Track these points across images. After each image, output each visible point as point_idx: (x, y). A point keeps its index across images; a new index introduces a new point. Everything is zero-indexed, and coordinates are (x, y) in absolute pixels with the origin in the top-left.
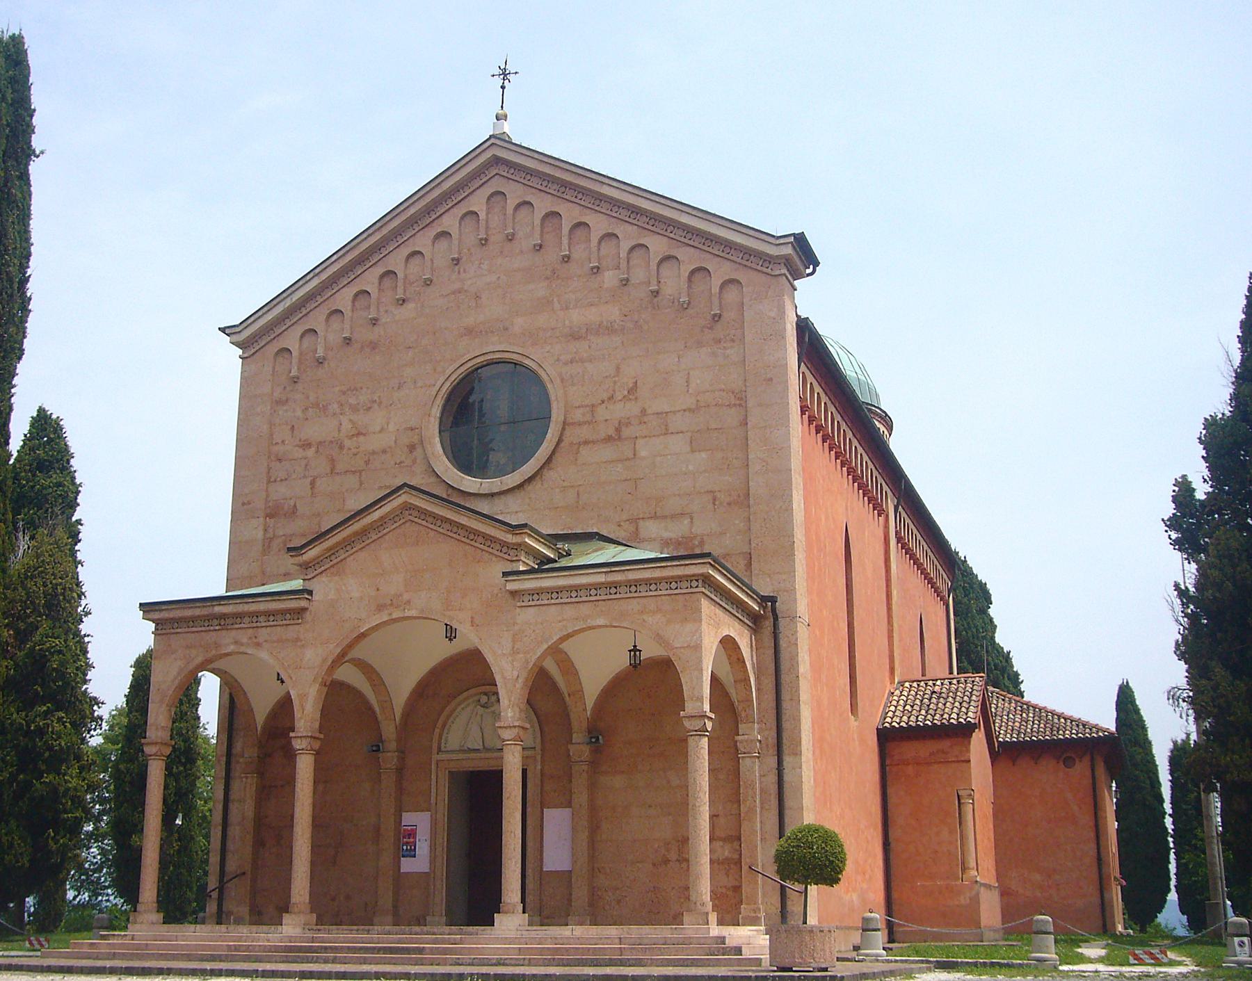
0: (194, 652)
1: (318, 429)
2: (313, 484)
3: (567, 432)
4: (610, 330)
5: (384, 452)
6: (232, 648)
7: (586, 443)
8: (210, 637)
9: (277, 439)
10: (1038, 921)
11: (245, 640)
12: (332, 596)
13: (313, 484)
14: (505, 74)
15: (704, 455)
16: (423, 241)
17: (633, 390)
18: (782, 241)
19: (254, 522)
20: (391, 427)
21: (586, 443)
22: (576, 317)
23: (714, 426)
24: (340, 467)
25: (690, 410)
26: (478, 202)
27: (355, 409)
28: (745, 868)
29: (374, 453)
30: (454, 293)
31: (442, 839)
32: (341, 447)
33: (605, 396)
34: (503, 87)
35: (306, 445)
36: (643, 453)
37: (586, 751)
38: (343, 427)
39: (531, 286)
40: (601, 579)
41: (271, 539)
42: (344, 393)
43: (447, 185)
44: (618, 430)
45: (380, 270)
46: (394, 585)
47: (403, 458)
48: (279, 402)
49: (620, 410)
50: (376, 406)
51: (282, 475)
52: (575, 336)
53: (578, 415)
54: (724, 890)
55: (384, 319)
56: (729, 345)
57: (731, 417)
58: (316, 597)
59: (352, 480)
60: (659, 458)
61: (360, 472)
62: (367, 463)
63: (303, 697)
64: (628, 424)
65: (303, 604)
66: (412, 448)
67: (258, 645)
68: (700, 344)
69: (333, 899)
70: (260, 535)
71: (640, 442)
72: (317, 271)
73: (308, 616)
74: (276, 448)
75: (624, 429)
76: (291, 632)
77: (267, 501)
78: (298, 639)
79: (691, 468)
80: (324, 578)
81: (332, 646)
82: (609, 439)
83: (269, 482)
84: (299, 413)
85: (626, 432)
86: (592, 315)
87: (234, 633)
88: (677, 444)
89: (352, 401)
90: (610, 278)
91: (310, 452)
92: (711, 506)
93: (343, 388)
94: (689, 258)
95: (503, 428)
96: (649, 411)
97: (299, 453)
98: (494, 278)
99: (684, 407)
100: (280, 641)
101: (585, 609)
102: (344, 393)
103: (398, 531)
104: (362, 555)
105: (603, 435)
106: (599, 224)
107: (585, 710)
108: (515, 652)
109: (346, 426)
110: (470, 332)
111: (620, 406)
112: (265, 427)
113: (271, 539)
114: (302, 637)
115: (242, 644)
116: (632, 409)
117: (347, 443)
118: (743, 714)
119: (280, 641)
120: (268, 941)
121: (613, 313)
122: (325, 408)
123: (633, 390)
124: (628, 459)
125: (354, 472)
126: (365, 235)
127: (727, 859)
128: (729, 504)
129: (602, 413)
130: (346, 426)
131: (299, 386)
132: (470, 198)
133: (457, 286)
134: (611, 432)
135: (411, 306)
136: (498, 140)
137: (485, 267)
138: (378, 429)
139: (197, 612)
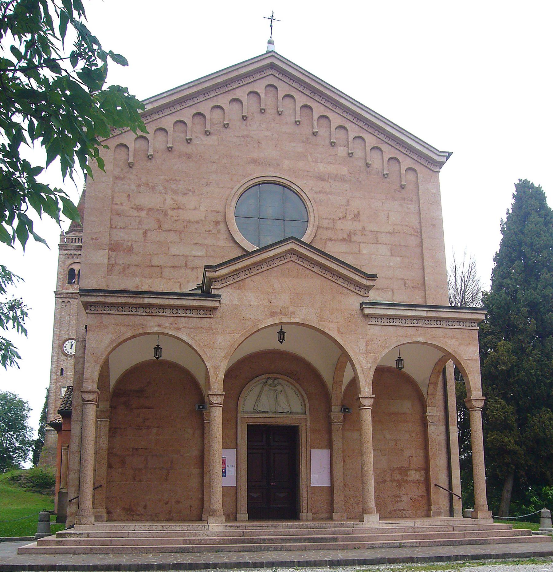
0: (123, 329)
1: (148, 200)
2: (145, 234)
3: (319, 233)
4: (343, 179)
5: (197, 222)
6: (156, 329)
7: (331, 240)
8: (138, 320)
9: (117, 200)
10: (544, 512)
11: (167, 325)
12: (236, 302)
13: (145, 234)
14: (272, 19)
15: (398, 259)
16: (223, 101)
17: (357, 215)
18: (442, 154)
19: (101, 252)
20: (202, 208)
21: (331, 240)
22: (322, 168)
23: (403, 244)
24: (165, 226)
25: (390, 233)
26: (260, 87)
27: (175, 192)
28: (432, 486)
29: (189, 222)
30: (243, 136)
31: (244, 466)
32: (166, 214)
33: (341, 215)
34: (271, 26)
35: (139, 209)
36: (364, 252)
37: (341, 415)
38: (167, 202)
39: (293, 144)
40: (424, 314)
41: (113, 265)
42: (167, 181)
43: (242, 71)
44: (349, 236)
45: (194, 111)
46: (283, 300)
47: (211, 228)
48: (117, 178)
49: (349, 225)
50: (191, 193)
51: (121, 224)
52: (322, 179)
53: (325, 223)
54: (416, 497)
55: (195, 142)
56: (409, 202)
57: (413, 241)
58: (223, 301)
59: (174, 237)
60: (373, 256)
61: (180, 232)
62: (185, 227)
63: (216, 368)
64: (355, 234)
65: (217, 304)
66: (217, 223)
67: (179, 329)
68: (393, 198)
69: (167, 503)
70: (106, 261)
71: (362, 245)
72: (152, 100)
73: (217, 313)
74: (116, 207)
75: (352, 236)
76: (205, 323)
77: (110, 240)
78: (210, 328)
79: (392, 264)
80: (229, 289)
81: (237, 336)
82: (344, 240)
83: (111, 228)
84: (134, 187)
85: (354, 238)
86: (332, 169)
87: (157, 319)
88: (384, 250)
89: (173, 186)
90: (341, 151)
91: (143, 214)
92: (403, 287)
93: (167, 178)
94: (389, 151)
95: (269, 222)
96: (367, 229)
97: (135, 213)
98: (269, 134)
99: (386, 231)
100: (196, 328)
101: (411, 331)
102: (167, 181)
103: (283, 266)
104: (258, 278)
105: (341, 238)
106: (336, 120)
107: (341, 393)
108: (367, 352)
109: (169, 202)
110: (254, 161)
111: (350, 223)
112: (109, 192)
113: (113, 265)
114: (213, 327)
115: (165, 328)
116: (357, 226)
117: (170, 213)
118: (430, 402)
119: (196, 328)
120: (207, 535)
121: (344, 171)
122: (153, 188)
123: (357, 215)
124: (356, 254)
125: (176, 232)
126: (186, 87)
127: (417, 480)
128: (413, 287)
129: (339, 225)
130: (169, 202)
131: (134, 171)
132: (254, 83)
133: (245, 133)
134: (345, 236)
135: (214, 137)
136: (271, 54)
137: (264, 126)
138: (192, 207)
139: (130, 301)
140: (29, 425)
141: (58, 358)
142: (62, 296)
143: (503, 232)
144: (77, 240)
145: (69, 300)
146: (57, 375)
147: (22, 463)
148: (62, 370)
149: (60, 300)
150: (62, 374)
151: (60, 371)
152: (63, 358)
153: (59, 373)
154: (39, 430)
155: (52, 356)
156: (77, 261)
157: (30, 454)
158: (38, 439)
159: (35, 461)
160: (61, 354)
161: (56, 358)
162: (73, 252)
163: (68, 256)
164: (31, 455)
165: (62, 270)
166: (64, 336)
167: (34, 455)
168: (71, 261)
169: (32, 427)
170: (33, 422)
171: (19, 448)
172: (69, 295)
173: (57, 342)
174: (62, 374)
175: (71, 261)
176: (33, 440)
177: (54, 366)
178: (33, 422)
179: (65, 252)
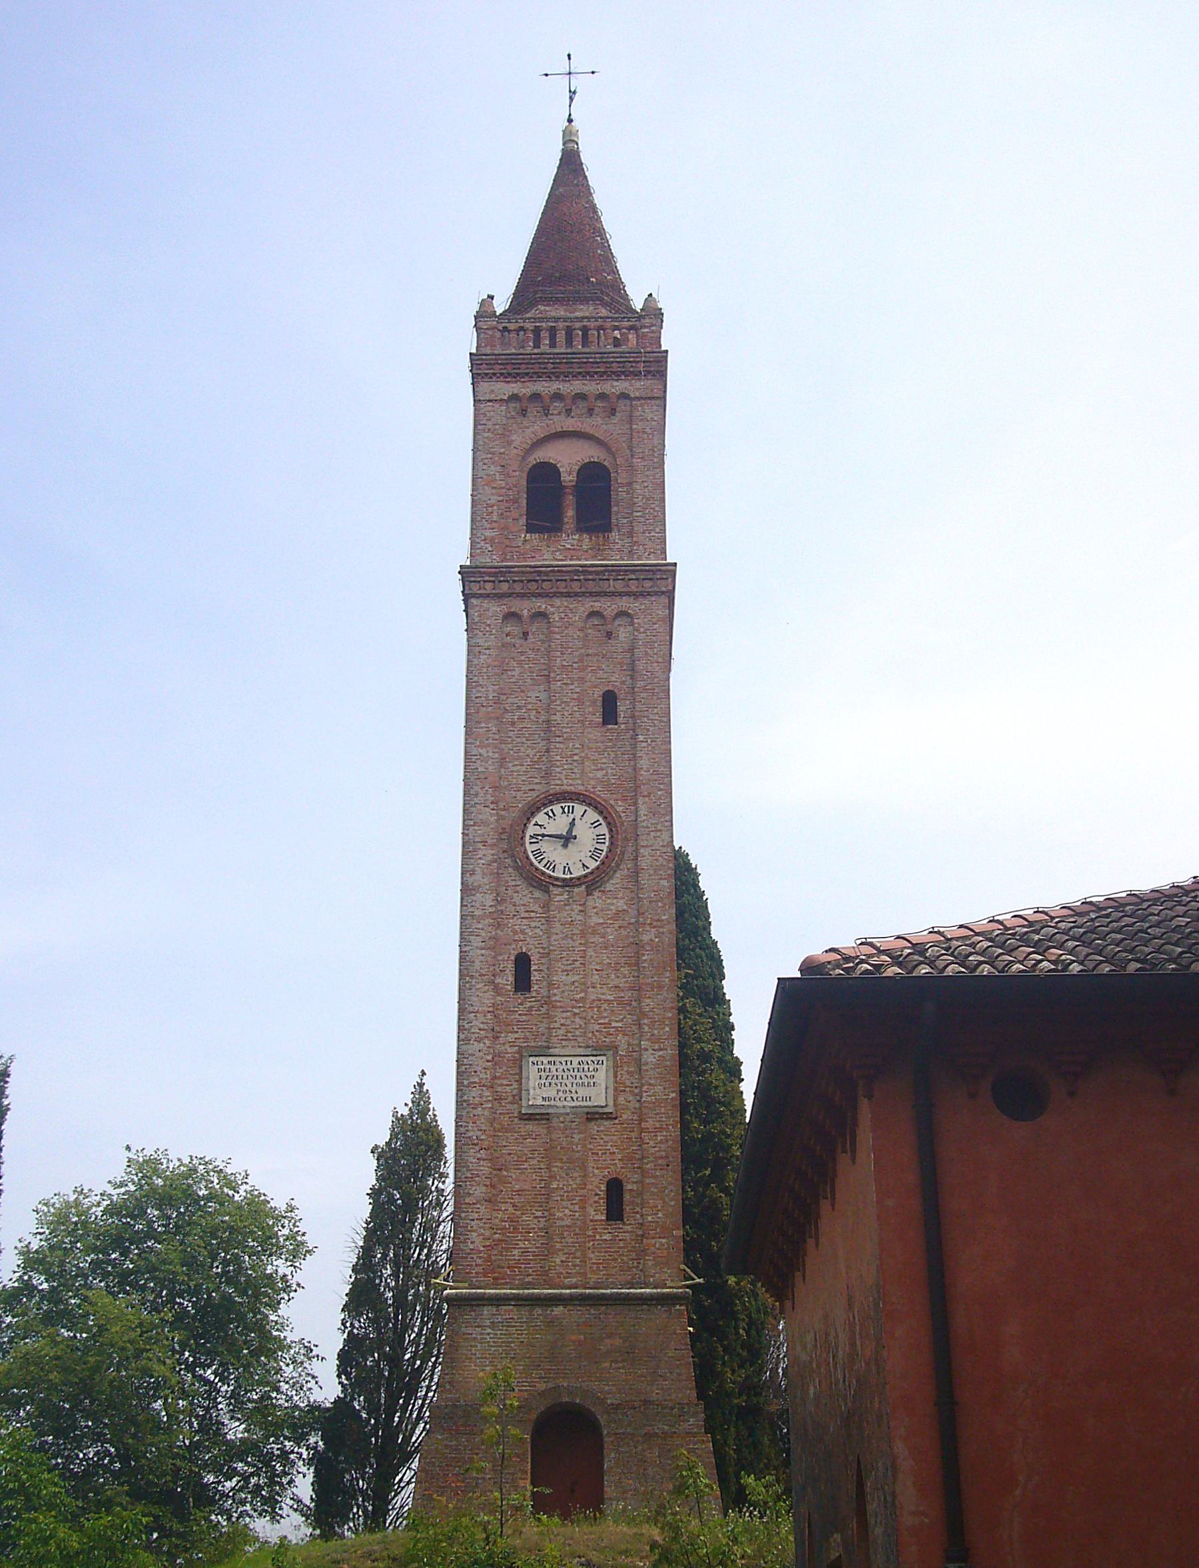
140: (290, 1336)
141: (499, 901)
142: (505, 587)
143: (808, 966)
144: (561, 337)
145: (541, 604)
146: (497, 989)
147: (261, 1526)
148: (523, 963)
149: (495, 609)
150: (523, 981)
151: (510, 966)
152: (525, 897)
153: (507, 979)
154: (343, 1356)
155: (467, 890)
156: (570, 424)
157: (299, 1479)
158: (338, 1401)
159: (326, 1512)
160: (511, 877)
161: (489, 900)
162: (545, 387)
163: (521, 405)
164: (304, 1486)
165: (493, 469)
166: (524, 784)
167: (320, 1485)
168: (536, 427)
169: (310, 1337)
170: (314, 1314)
171: (242, 1450)
172: (540, 582)
173: (487, 814)
174: (523, 981)
175: (536, 427)
176: (314, 1408)
177: (476, 942)
178: (314, 1314)
179: (505, 389)
